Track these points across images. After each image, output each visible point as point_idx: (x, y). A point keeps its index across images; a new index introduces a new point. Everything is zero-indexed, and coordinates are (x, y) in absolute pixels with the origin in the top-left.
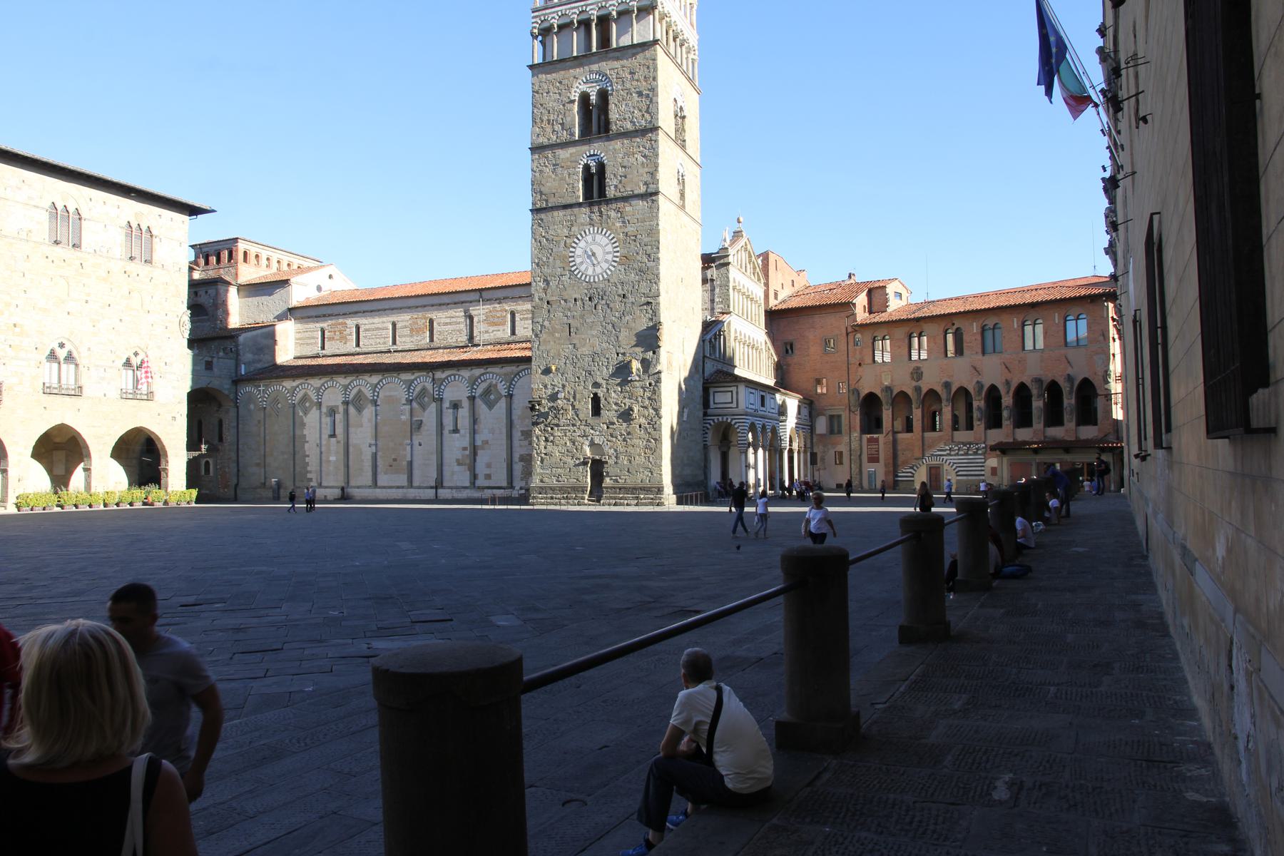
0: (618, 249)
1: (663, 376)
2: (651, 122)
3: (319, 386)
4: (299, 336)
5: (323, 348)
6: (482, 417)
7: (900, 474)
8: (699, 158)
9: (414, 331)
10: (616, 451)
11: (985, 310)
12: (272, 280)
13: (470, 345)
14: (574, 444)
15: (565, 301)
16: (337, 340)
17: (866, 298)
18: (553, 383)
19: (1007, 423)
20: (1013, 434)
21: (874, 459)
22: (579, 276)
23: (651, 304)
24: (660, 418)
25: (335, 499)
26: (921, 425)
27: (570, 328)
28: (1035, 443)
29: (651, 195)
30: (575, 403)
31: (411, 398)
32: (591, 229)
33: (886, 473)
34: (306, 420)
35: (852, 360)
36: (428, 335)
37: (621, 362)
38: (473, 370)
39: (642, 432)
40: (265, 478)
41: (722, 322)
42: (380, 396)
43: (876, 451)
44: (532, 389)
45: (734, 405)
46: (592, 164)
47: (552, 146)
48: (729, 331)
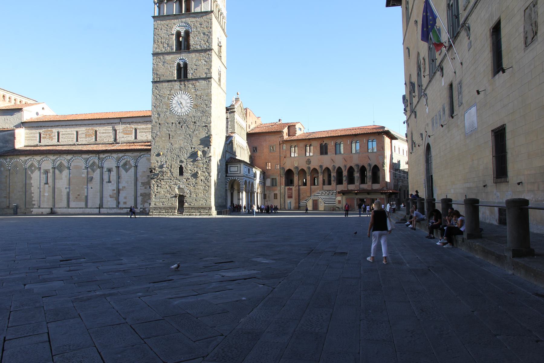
0: (193, 101)
1: (212, 158)
2: (209, 46)
3: (39, 159)
4: (27, 136)
5: (40, 142)
6: (122, 176)
7: (301, 203)
8: (226, 65)
9: (87, 136)
10: (190, 191)
11: (337, 136)
12: (13, 108)
13: (115, 143)
14: (171, 188)
15: (168, 123)
16: (47, 138)
17: (287, 130)
18: (161, 160)
19: (345, 182)
20: (347, 186)
21: (290, 197)
22: (174, 113)
23: (207, 126)
24: (211, 177)
25: (48, 214)
26: (310, 183)
27: (169, 136)
28: (356, 191)
29: (208, 79)
30: (171, 170)
31: (87, 166)
32: (180, 92)
33: (295, 203)
34: (32, 176)
35: (282, 155)
36: (94, 138)
37: (193, 152)
38: (118, 154)
39: (202, 183)
40: (9, 204)
41: (232, 137)
42: (72, 165)
43: (291, 193)
44: (151, 163)
45: (239, 172)
46: (181, 63)
47: (163, 54)
48: (234, 141)
